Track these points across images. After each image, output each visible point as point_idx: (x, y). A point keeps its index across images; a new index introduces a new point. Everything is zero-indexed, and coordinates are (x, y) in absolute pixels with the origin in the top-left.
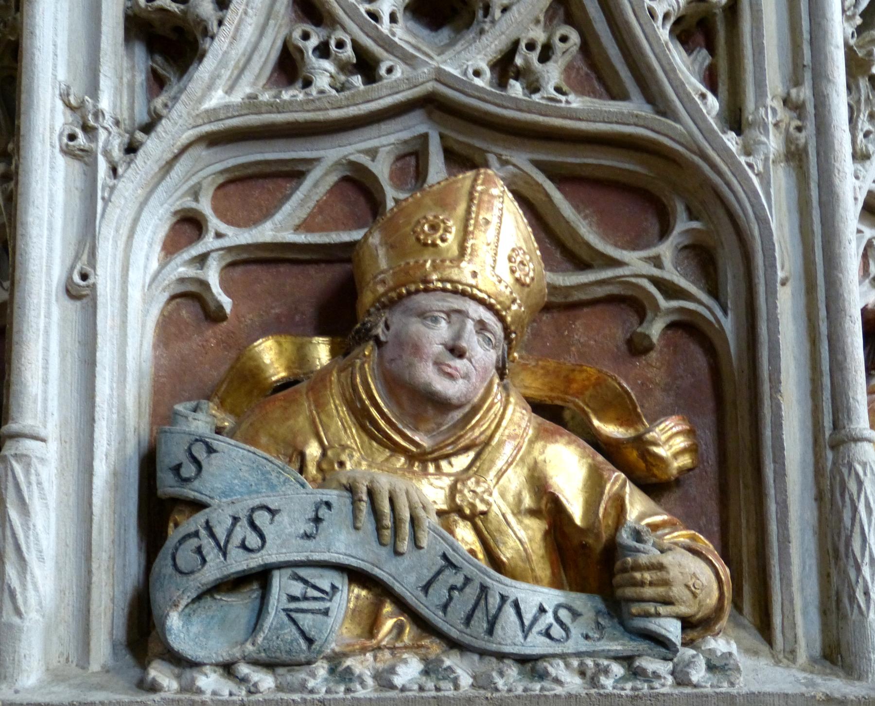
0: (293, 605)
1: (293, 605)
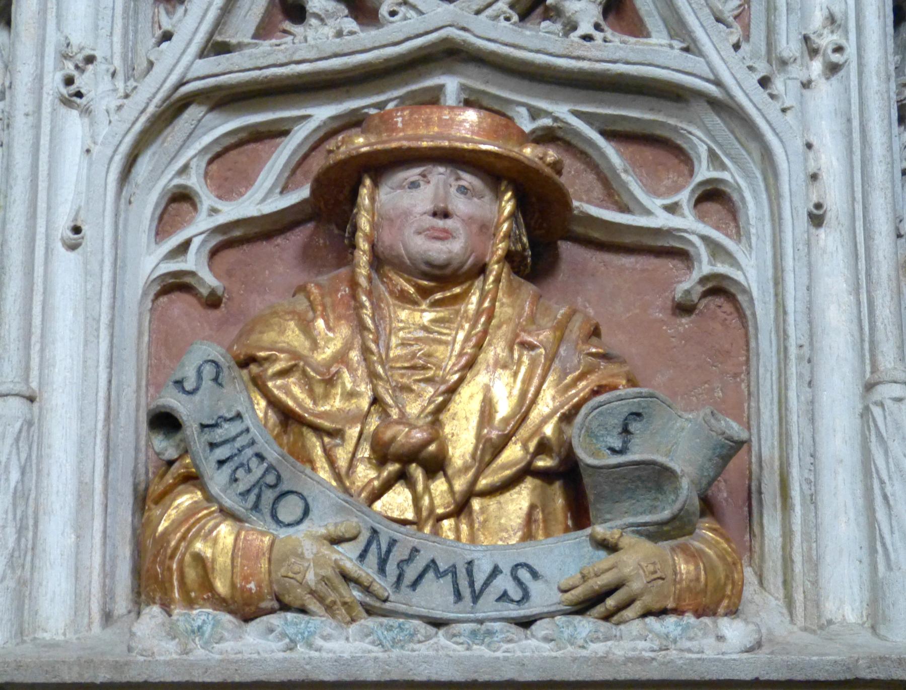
0: (466, 592)
1: (466, 592)
